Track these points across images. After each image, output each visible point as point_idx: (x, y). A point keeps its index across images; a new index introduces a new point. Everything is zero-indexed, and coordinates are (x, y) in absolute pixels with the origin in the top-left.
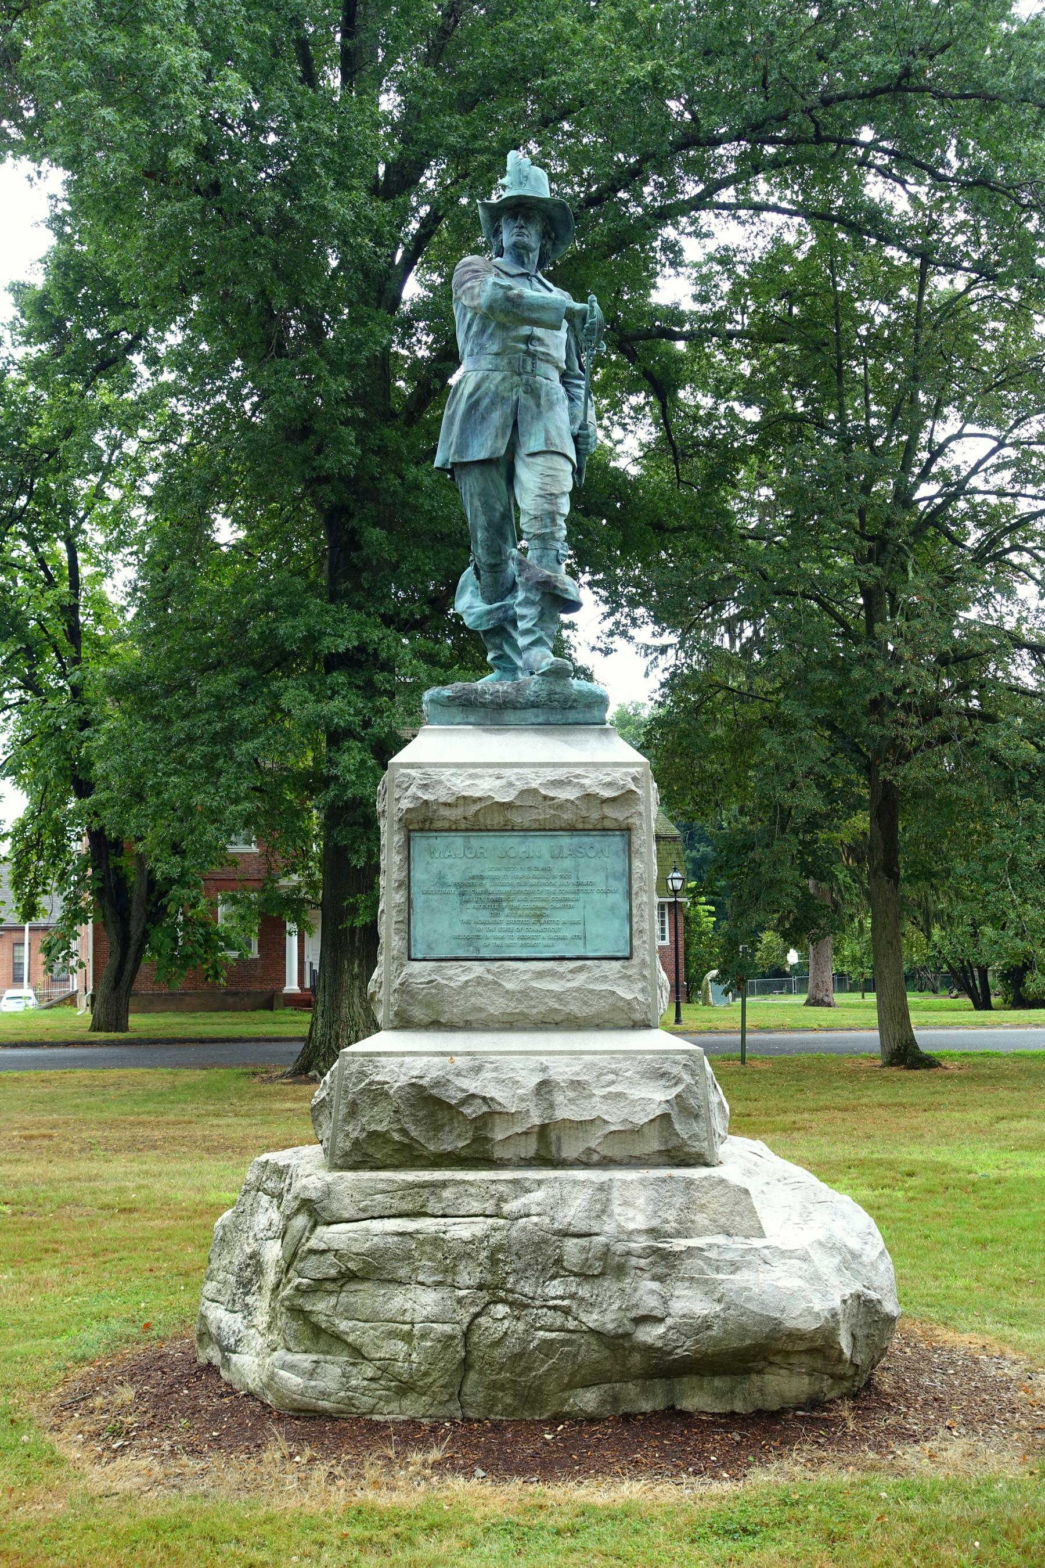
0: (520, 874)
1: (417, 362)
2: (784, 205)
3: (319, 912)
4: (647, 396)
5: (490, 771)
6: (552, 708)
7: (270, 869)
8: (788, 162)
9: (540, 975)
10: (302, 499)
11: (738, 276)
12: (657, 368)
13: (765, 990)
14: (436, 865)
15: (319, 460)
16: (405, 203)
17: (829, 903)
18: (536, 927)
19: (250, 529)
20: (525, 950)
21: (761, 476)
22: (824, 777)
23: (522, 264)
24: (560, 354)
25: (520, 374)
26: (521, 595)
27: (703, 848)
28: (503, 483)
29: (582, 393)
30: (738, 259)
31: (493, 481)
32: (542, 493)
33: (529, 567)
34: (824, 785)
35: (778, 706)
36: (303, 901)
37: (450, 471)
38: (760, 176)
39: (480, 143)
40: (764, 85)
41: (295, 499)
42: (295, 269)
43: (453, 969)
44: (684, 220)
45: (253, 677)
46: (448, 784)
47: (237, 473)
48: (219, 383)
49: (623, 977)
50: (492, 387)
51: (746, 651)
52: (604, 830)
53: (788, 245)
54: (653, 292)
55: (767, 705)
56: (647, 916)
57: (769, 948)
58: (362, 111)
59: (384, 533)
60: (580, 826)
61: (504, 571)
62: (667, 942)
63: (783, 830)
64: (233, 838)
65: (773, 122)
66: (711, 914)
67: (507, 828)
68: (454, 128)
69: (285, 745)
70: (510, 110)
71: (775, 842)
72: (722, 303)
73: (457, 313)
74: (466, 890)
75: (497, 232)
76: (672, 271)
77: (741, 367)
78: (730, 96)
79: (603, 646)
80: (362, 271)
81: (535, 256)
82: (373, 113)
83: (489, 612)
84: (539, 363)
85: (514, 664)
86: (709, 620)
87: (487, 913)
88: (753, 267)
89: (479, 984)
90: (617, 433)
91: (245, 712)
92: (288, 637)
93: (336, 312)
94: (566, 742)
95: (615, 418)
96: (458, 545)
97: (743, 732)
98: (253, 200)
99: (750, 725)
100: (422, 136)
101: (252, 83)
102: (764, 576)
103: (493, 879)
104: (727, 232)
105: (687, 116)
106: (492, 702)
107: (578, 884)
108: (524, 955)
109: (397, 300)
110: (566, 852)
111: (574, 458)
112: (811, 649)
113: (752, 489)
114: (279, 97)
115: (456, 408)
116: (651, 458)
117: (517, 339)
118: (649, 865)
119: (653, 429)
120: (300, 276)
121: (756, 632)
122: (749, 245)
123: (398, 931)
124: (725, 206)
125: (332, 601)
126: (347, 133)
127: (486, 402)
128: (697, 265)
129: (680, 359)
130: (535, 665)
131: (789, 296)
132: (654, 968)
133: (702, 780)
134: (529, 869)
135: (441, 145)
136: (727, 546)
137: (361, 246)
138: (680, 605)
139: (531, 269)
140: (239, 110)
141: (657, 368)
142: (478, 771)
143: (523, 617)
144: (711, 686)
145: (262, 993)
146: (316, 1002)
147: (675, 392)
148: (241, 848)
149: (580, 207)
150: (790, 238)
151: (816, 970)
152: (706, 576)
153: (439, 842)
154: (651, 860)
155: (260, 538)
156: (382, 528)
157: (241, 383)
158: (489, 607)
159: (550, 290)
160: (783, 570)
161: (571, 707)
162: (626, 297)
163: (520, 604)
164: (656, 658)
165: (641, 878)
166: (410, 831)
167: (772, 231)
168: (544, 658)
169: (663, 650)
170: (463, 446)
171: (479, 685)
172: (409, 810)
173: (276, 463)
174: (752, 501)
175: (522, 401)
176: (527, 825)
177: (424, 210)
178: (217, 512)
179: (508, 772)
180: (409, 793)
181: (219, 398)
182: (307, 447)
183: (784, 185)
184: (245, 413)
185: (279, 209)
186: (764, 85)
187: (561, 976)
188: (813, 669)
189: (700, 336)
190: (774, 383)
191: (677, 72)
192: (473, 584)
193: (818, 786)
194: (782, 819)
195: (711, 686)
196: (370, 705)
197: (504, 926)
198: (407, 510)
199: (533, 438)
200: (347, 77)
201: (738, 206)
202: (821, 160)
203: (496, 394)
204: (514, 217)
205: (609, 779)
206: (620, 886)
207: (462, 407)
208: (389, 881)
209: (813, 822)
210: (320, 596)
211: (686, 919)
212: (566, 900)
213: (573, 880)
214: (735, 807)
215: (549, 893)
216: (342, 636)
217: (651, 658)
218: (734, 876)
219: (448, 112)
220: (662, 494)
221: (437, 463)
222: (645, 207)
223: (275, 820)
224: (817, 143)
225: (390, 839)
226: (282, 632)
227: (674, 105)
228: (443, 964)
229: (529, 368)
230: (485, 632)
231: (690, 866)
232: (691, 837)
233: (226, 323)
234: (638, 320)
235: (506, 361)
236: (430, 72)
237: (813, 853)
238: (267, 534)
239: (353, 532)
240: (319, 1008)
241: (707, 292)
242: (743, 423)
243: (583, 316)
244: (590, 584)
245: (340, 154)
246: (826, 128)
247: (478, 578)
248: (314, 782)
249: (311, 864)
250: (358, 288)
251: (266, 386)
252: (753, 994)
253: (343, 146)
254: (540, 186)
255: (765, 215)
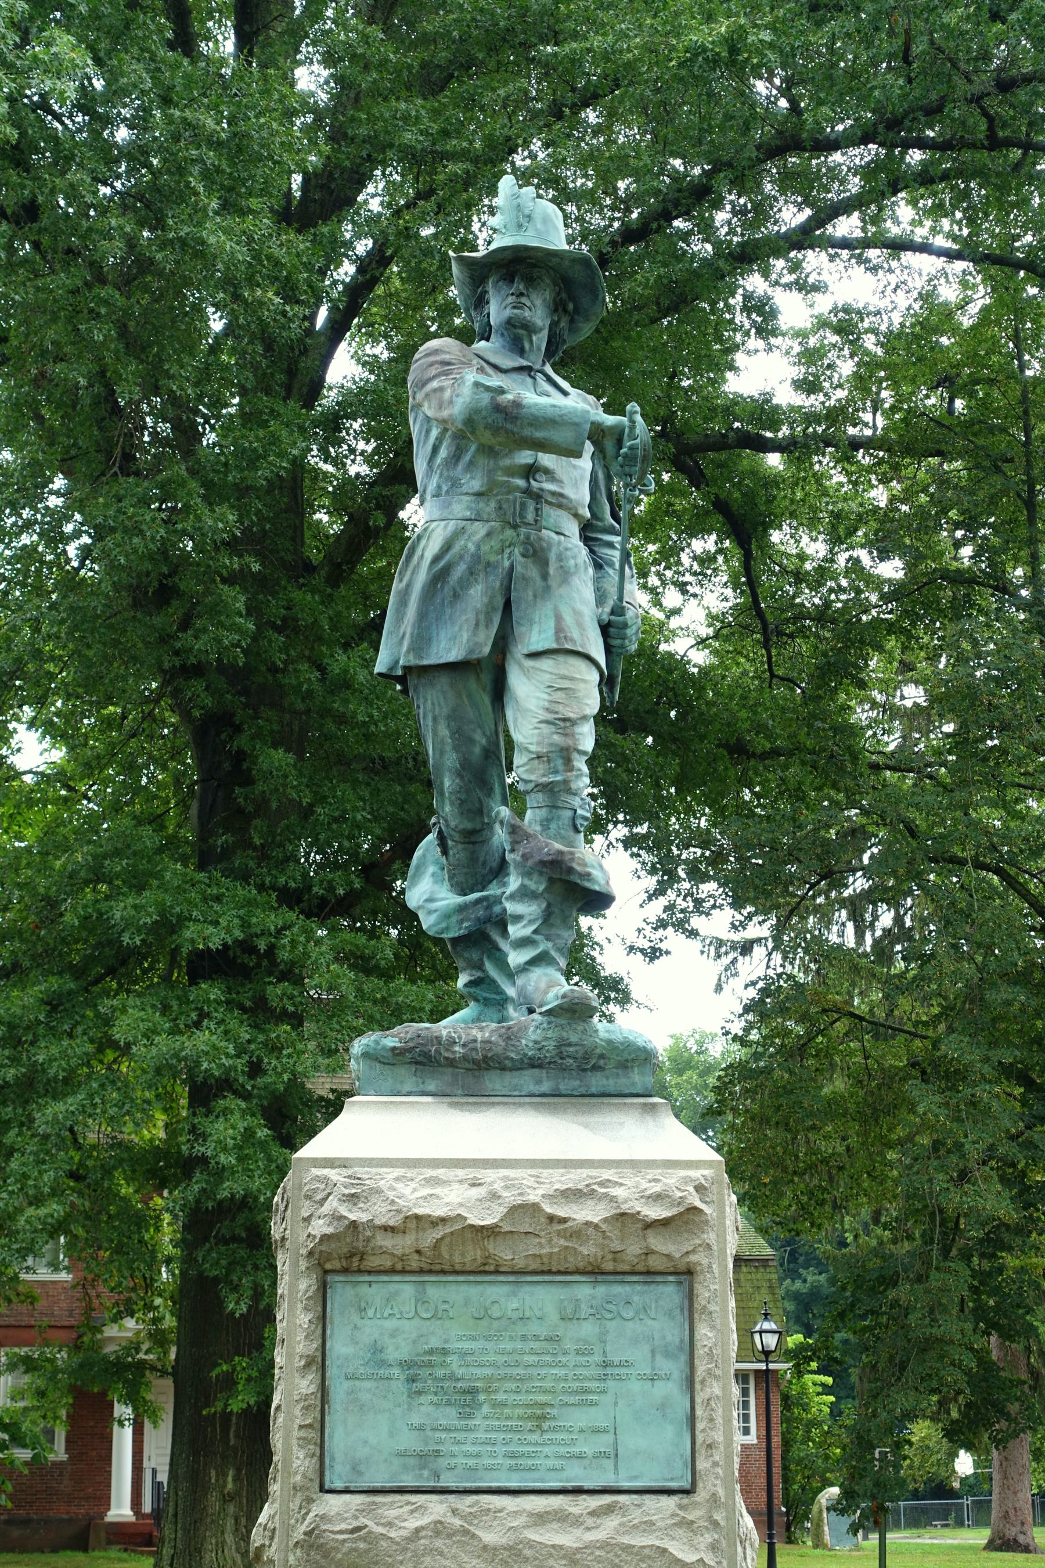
0: (509, 1346)
1: (349, 484)
2: (940, 241)
3: (168, 1383)
4: (720, 540)
5: (461, 1173)
6: (564, 1069)
7: (89, 1309)
8: (945, 177)
9: (540, 1519)
10: (157, 702)
11: (867, 352)
12: (737, 495)
13: (918, 1520)
14: (370, 1330)
15: (186, 639)
16: (333, 234)
17: (1024, 1376)
18: (535, 1437)
19: (71, 749)
20: (515, 1476)
21: (906, 667)
22: (1013, 1165)
23: (521, 352)
24: (581, 495)
25: (515, 527)
26: (514, 882)
27: (813, 1278)
28: (487, 700)
29: (616, 555)
30: (866, 324)
31: (470, 696)
32: (550, 717)
33: (528, 836)
34: (1015, 1180)
35: (935, 1045)
36: (142, 1365)
37: (402, 680)
38: (902, 195)
39: (453, 144)
40: (906, 60)
41: (147, 701)
42: (153, 339)
43: (394, 1508)
44: (779, 264)
45: (70, 993)
46: (391, 1195)
47: (52, 658)
48: (26, 513)
49: (680, 1524)
50: (471, 547)
51: (882, 952)
52: (648, 1273)
53: (946, 304)
54: (729, 375)
55: (918, 1043)
56: (719, 1420)
57: (925, 1449)
58: (266, 92)
59: (291, 758)
60: (609, 1266)
61: (486, 841)
62: (752, 1439)
63: (945, 1252)
64: (30, 1261)
65: (919, 114)
66: (827, 1390)
67: (488, 1270)
68: (415, 119)
69: (120, 1105)
70: (502, 92)
71: (933, 1273)
72: (841, 394)
73: (415, 429)
74: (419, 1373)
75: (480, 302)
76: (760, 344)
77: (873, 493)
78: (852, 74)
79: (647, 945)
80: (263, 340)
81: (541, 340)
82: (283, 98)
83: (461, 909)
84: (546, 508)
85: (502, 992)
86: (820, 900)
87: (452, 1412)
88: (891, 340)
89: (437, 1534)
90: (672, 598)
91: (54, 1050)
92: (128, 923)
93: (218, 403)
94: (586, 1126)
95: (669, 574)
96: (411, 779)
97: (879, 1087)
98: (90, 229)
99: (890, 1077)
100: (363, 131)
101: (92, 48)
102: (912, 832)
103: (463, 1354)
104: (848, 284)
105: (783, 103)
106: (465, 1058)
107: (606, 1365)
108: (513, 1485)
109: (316, 386)
110: (585, 1310)
111: (602, 661)
112: (989, 948)
113: (888, 686)
114: (135, 71)
115: (412, 579)
116: (727, 639)
117: (511, 471)
118: (723, 1333)
119: (729, 592)
120: (162, 348)
121: (898, 920)
122: (884, 304)
123: (304, 1442)
124: (845, 244)
125: (201, 867)
126: (242, 126)
127: (460, 570)
128: (801, 335)
129: (772, 482)
130: (537, 998)
131: (948, 382)
132: (732, 1510)
133: (811, 1167)
134: (524, 1338)
135: (391, 146)
136: (850, 783)
137: (261, 304)
138: (776, 880)
139: (536, 359)
140: (71, 89)
141: (737, 495)
142: (440, 1172)
143: (517, 918)
144: (824, 1011)
145: (70, 1521)
146: (162, 1540)
147: (766, 534)
148: (44, 1274)
149: (613, 243)
150: (949, 293)
151: (1003, 1487)
152: (816, 830)
153: (375, 1291)
154: (726, 1324)
155: (87, 765)
156: (287, 750)
157: (61, 517)
158: (461, 900)
159: (565, 394)
160: (943, 820)
161: (596, 1068)
162: (685, 383)
163: (512, 897)
164: (734, 961)
165: (710, 1355)
166: (326, 1272)
167: (918, 283)
168: (552, 985)
169: (746, 948)
170: (422, 640)
171: (445, 1027)
172: (325, 1238)
173: (115, 643)
174: (892, 707)
175: (519, 569)
176: (520, 1264)
177: (363, 246)
178: (18, 720)
179: (490, 1175)
180: (326, 1209)
181: (26, 539)
182: (167, 618)
183: (938, 211)
184: (68, 561)
185: (132, 243)
186: (906, 60)
187: (576, 1522)
188: (993, 985)
189: (806, 446)
190: (925, 523)
191: (768, 38)
192: (437, 862)
193: (1003, 1179)
194: (944, 1234)
195: (824, 1011)
196: (261, 1038)
197: (481, 1435)
198: (329, 720)
199: (536, 628)
200: (244, 40)
201: (867, 243)
202: (998, 175)
203: (477, 558)
204: (509, 279)
205: (657, 1188)
206: (675, 1368)
207: (421, 578)
208: (290, 1356)
209: (997, 1238)
210: (184, 860)
211: (786, 1398)
212: (586, 1391)
213: (597, 1358)
214: (866, 1213)
215: (558, 1379)
216: (216, 923)
217: (726, 960)
218: (864, 1329)
219: (404, 93)
220: (744, 698)
221: (380, 667)
222: (717, 244)
223: (105, 1233)
224: (991, 149)
225: (293, 1286)
226: (118, 915)
227: (761, 87)
228: (379, 1499)
229: (530, 517)
230: (455, 941)
231: (790, 1306)
232: (793, 1256)
233: (40, 419)
234: (706, 419)
235: (493, 505)
236: (376, 32)
237: (996, 1291)
238: (98, 757)
239: (240, 756)
240: (167, 1551)
241: (817, 377)
242: (875, 582)
243: (618, 435)
244: (628, 843)
245: (230, 159)
246: (1004, 125)
247: (445, 852)
248: (165, 1167)
249: (158, 1301)
250: (255, 367)
251: (100, 520)
252: (897, 1526)
253: (236, 147)
254: (551, 229)
255: (908, 257)
